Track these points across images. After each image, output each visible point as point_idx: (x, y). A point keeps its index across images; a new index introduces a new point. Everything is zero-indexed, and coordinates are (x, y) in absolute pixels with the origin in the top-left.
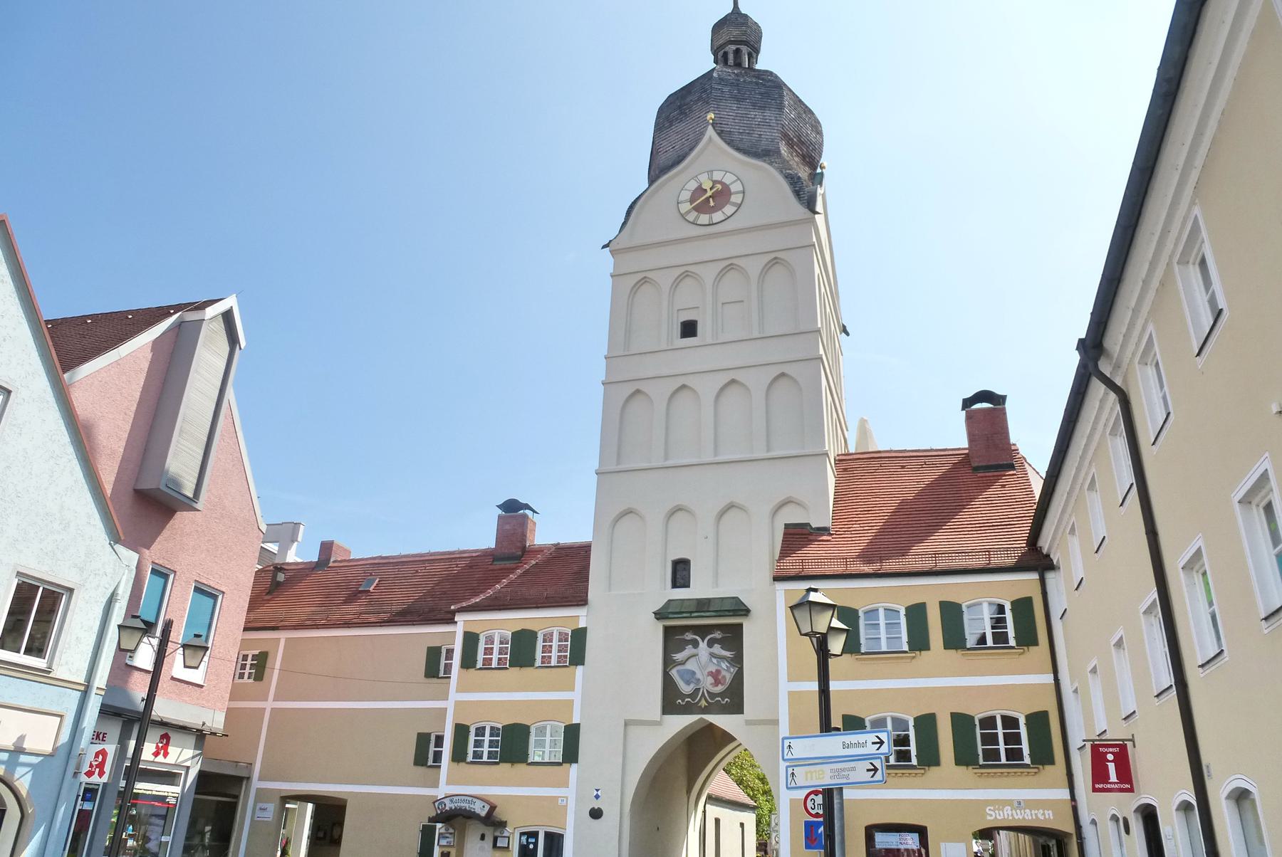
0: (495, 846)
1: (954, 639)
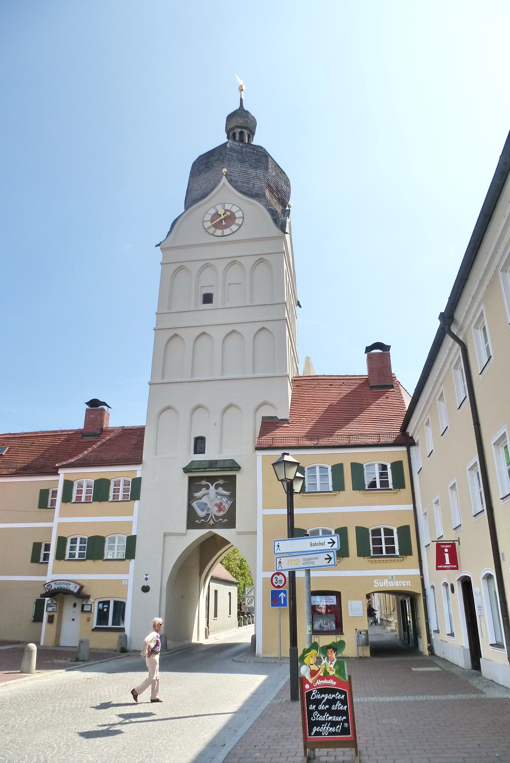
0: (82, 610)
1: (359, 485)
